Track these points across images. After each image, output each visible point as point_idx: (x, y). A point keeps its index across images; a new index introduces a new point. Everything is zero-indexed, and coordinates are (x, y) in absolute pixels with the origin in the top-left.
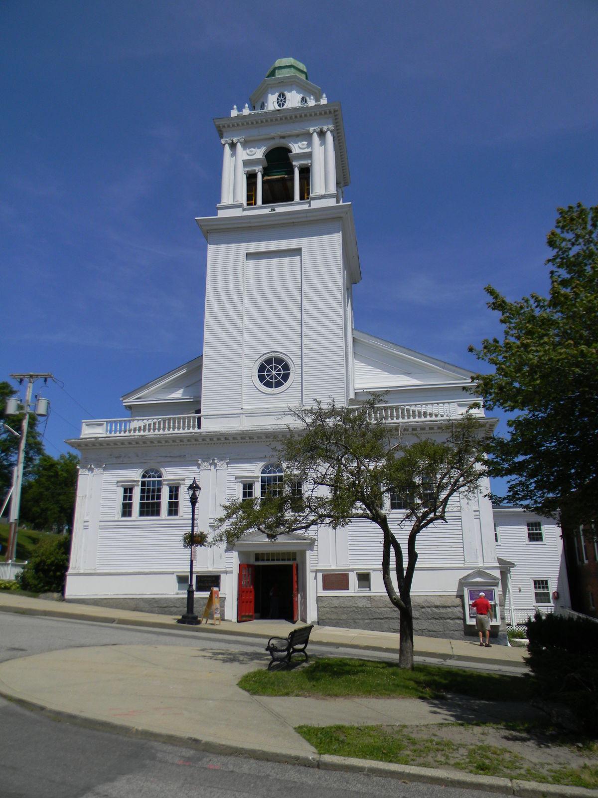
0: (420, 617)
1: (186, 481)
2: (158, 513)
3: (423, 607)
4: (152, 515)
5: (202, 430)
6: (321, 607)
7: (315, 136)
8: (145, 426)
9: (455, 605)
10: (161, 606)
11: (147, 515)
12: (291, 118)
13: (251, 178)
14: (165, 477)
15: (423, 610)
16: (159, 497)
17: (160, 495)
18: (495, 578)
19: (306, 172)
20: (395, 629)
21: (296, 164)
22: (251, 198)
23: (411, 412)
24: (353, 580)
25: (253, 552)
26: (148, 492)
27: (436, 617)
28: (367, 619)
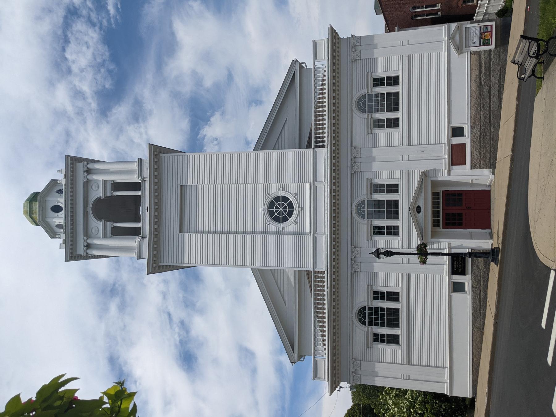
0: (489, 85)
1: (369, 178)
2: (397, 310)
3: (481, 83)
4: (398, 315)
5: (325, 270)
6: (480, 167)
7: (89, 177)
8: (320, 326)
9: (478, 59)
10: (479, 307)
11: (398, 320)
12: (72, 167)
13: (117, 232)
14: (365, 304)
15: (483, 83)
16: (382, 202)
17: (379, 300)
18: (457, 28)
19: (117, 186)
20: (499, 106)
21: (109, 193)
22: (136, 232)
23: (320, 96)
24: (457, 140)
25: (431, 228)
26: (376, 314)
27: (488, 73)
28: (490, 129)
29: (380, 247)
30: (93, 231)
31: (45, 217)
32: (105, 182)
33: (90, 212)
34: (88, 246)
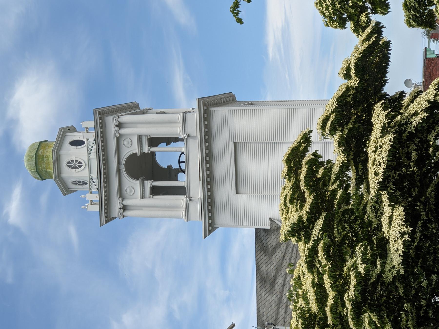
7: (123, 131)
29: (237, 141)
30: (128, 190)
31: (61, 174)
32: (140, 137)
33: (123, 170)
34: (125, 208)
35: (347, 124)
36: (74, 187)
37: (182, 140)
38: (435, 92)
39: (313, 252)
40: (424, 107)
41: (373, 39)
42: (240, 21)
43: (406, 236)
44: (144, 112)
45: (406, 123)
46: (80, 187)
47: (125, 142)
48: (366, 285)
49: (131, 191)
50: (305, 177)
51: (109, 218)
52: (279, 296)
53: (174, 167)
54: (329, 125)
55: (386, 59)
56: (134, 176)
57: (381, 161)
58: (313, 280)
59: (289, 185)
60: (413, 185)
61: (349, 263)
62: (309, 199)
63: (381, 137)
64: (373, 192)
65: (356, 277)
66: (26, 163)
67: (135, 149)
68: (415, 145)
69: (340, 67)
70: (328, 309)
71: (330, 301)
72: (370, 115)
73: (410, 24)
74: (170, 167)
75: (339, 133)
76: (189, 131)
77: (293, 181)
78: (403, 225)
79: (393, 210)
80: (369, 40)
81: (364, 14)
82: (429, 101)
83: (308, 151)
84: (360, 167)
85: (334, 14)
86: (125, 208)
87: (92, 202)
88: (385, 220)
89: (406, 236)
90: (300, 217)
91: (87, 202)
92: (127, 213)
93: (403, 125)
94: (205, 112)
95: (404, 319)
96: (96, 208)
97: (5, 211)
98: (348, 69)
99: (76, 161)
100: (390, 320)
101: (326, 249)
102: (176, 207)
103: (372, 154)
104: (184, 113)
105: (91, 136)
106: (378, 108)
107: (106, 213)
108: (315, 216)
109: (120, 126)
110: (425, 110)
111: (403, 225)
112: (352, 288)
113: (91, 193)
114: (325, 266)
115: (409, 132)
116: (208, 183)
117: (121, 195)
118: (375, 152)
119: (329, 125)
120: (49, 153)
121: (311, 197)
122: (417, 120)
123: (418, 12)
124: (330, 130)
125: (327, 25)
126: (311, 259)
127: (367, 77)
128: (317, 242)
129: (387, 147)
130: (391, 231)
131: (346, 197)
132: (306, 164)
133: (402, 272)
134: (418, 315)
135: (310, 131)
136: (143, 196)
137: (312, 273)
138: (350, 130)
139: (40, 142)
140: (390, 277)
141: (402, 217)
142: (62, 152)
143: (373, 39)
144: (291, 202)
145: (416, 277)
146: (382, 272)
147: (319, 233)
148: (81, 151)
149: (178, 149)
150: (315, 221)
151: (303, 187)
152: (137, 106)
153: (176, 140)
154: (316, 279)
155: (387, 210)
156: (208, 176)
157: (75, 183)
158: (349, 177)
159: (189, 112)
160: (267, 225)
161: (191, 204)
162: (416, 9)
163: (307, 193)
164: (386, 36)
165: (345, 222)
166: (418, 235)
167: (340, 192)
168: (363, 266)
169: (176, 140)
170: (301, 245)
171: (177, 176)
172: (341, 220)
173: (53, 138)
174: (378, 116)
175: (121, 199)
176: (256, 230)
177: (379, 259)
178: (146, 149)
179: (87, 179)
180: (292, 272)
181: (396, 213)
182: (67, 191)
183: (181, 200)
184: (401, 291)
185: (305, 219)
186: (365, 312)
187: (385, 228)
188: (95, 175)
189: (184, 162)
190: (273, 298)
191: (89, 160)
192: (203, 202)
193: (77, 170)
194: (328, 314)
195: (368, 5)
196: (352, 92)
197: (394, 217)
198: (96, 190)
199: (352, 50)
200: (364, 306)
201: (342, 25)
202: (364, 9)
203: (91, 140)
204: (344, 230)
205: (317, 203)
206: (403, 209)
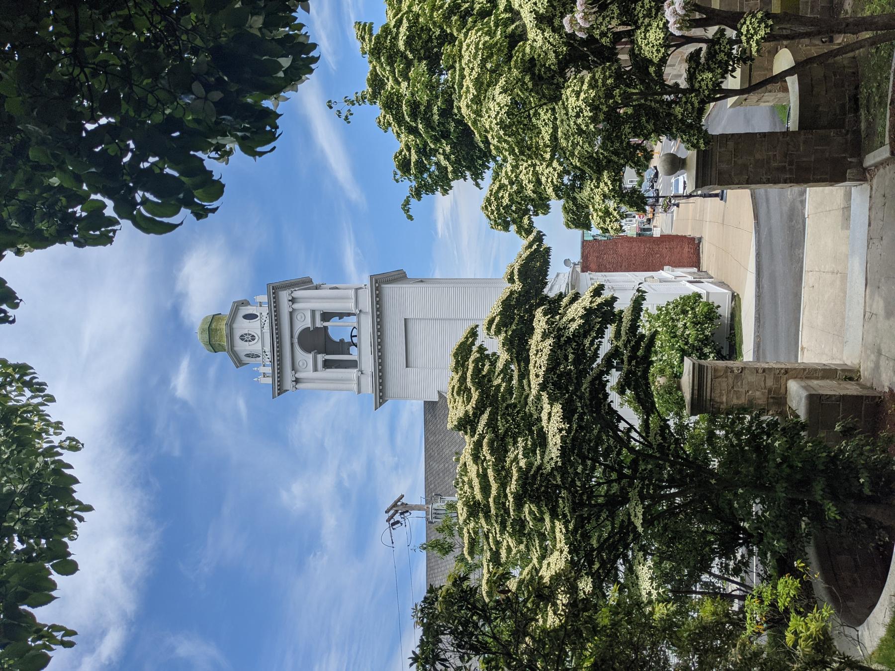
7: (296, 306)
30: (301, 364)
34: (297, 381)
35: (511, 324)
36: (246, 360)
37: (354, 314)
38: (590, 299)
39: (478, 445)
40: (580, 314)
41: (535, 247)
42: (410, 218)
43: (564, 432)
44: (317, 288)
45: (565, 328)
46: (253, 359)
47: (298, 317)
48: (527, 478)
49: (303, 364)
50: (471, 375)
51: (281, 391)
52: (446, 465)
53: (346, 341)
54: (494, 327)
55: (546, 263)
56: (307, 350)
57: (542, 364)
58: (478, 470)
59: (457, 377)
60: (569, 381)
61: (511, 455)
62: (475, 395)
63: (541, 341)
64: (534, 392)
65: (517, 471)
66: (199, 336)
67: (308, 324)
68: (573, 349)
69: (504, 272)
70: (491, 500)
71: (494, 492)
72: (531, 320)
73: (568, 227)
74: (342, 341)
75: (503, 335)
76: (361, 307)
77: (460, 373)
78: (561, 422)
79: (552, 407)
80: (531, 248)
81: (527, 217)
82: (585, 309)
83: (474, 345)
84: (522, 364)
85: (499, 219)
86: (297, 381)
87: (264, 375)
88: (544, 416)
89: (564, 432)
90: (466, 411)
91: (260, 374)
92: (299, 386)
93: (561, 329)
94: (377, 289)
95: (561, 506)
96: (269, 381)
97: (172, 385)
98: (512, 273)
99: (249, 334)
100: (548, 509)
101: (491, 444)
102: (349, 380)
103: (534, 357)
104: (357, 290)
105: (265, 310)
106: (539, 313)
107: (278, 386)
108: (480, 410)
109: (293, 300)
110: (581, 317)
111: (561, 422)
112: (514, 482)
113: (264, 366)
114: (489, 461)
115: (567, 337)
116: (380, 357)
117: (294, 368)
118: (536, 355)
119: (494, 327)
120: (223, 326)
121: (477, 393)
122: (574, 326)
123: (576, 215)
124: (495, 333)
125: (492, 227)
126: (476, 452)
127: (529, 281)
128: (482, 437)
129: (547, 351)
130: (550, 427)
131: (510, 391)
132: (473, 362)
133: (560, 464)
134: (574, 502)
135: (477, 326)
136: (315, 369)
137: (477, 464)
138: (513, 331)
139: (214, 315)
140: (549, 468)
141: (560, 414)
142: (235, 326)
143: (535, 247)
144: (458, 394)
145: (572, 465)
146: (542, 464)
147: (484, 428)
148: (253, 327)
149: (350, 324)
150: (481, 415)
151: (469, 384)
152: (310, 281)
153: (349, 315)
154: (481, 471)
155: (546, 407)
156: (379, 351)
157: (248, 355)
158: (513, 371)
159: (361, 288)
160: (436, 398)
161: (363, 379)
162: (574, 212)
163: (473, 389)
164: (546, 242)
165: (508, 415)
166: (575, 426)
167: (504, 384)
168: (524, 461)
169: (349, 315)
170: (467, 438)
171: (349, 349)
172: (504, 414)
173: (226, 311)
174: (539, 321)
175: (293, 372)
176: (425, 402)
177: (538, 448)
178: (319, 324)
179: (260, 352)
180: (458, 460)
181: (554, 410)
182: (240, 363)
183: (353, 373)
184: (559, 479)
185: (471, 413)
186: (525, 503)
187: (544, 423)
188: (268, 348)
189: (356, 336)
190: (440, 467)
191: (262, 333)
192: (374, 376)
193: (250, 343)
194: (492, 505)
195: (530, 207)
196: (516, 295)
197: (553, 414)
198: (269, 363)
199: (515, 256)
200: (525, 497)
201: (506, 228)
202: (526, 212)
203: (265, 314)
204: (507, 423)
205: (482, 399)
206: (561, 406)
